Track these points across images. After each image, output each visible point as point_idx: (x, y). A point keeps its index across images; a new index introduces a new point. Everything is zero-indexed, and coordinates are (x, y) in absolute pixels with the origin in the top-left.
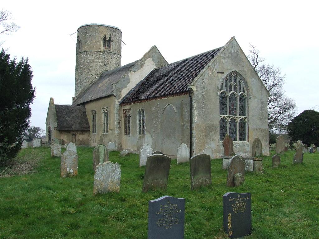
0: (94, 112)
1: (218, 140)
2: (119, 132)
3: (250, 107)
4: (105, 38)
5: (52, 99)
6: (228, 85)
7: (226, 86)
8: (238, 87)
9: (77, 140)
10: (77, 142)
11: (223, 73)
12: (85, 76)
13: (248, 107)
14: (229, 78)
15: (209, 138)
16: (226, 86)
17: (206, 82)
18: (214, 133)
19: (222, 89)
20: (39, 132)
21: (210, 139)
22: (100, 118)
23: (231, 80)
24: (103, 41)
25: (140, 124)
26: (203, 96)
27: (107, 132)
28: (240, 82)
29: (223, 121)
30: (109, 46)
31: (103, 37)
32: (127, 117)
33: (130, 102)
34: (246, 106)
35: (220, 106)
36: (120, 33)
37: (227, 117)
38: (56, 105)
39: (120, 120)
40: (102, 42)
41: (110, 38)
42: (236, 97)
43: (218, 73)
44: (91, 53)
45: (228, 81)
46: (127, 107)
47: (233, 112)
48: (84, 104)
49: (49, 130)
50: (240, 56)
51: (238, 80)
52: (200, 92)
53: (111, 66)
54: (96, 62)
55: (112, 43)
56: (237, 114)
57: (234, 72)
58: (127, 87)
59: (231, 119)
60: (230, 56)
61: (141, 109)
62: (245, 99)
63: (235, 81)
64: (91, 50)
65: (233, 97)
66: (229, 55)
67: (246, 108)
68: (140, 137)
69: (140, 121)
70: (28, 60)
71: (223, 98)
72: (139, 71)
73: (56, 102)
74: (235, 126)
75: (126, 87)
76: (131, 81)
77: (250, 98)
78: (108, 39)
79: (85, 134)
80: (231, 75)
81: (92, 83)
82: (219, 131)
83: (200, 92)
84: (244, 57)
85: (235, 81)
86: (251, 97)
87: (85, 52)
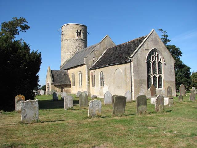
21: (142, 88)
25: (101, 80)
26: (138, 63)
32: (94, 77)
43: (146, 50)
69: (101, 78)
78: (79, 32)
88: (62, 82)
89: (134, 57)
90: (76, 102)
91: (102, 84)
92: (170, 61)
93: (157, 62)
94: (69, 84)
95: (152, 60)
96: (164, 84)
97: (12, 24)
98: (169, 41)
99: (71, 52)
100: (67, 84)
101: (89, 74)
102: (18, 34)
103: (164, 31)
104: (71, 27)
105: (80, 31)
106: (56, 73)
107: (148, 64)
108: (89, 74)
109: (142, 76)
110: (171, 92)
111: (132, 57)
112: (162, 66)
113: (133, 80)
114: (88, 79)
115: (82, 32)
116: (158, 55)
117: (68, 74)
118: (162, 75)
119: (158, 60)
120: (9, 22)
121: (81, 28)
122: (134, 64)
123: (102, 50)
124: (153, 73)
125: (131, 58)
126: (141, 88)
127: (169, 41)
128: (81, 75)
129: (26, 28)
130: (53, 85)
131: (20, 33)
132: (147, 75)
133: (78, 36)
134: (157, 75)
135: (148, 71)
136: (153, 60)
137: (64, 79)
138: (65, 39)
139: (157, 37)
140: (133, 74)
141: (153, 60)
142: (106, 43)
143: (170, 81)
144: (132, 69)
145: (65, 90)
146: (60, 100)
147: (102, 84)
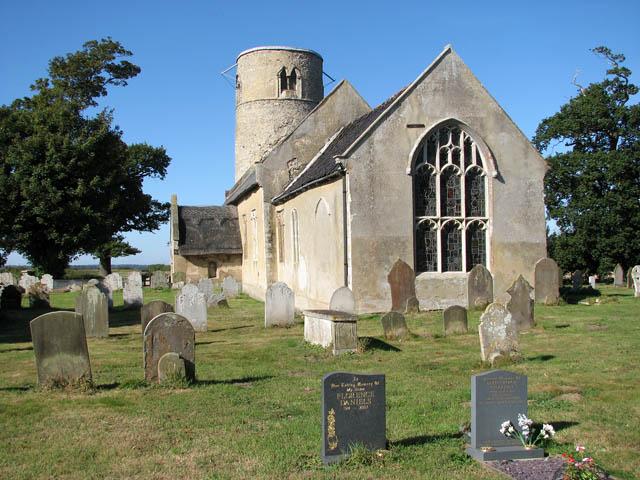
26: (372, 179)
43: (409, 126)
78: (288, 74)
88: (213, 246)
89: (353, 156)
91: (296, 259)
92: (526, 165)
93: (462, 171)
94: (234, 252)
95: (465, 168)
96: (492, 257)
97: (79, 61)
98: (633, 90)
100: (227, 252)
101: (271, 218)
102: (105, 93)
103: (614, 52)
104: (260, 59)
105: (293, 72)
106: (195, 216)
107: (421, 182)
108: (271, 218)
109: (388, 228)
110: (488, 289)
111: (346, 157)
112: (488, 185)
114: (270, 235)
115: (298, 75)
116: (468, 144)
117: (237, 219)
118: (485, 221)
119: (468, 162)
121: (296, 60)
122: (354, 181)
123: (324, 132)
124: (442, 215)
125: (343, 161)
127: (633, 90)
129: (127, 71)
130: (180, 257)
131: (108, 87)
132: (416, 221)
133: (284, 87)
134: (461, 221)
135: (421, 204)
136: (443, 160)
137: (219, 236)
138: (243, 101)
139: (463, 76)
141: (443, 160)
142: (338, 108)
143: (524, 243)
145: (222, 272)
146: (27, 309)
147: (296, 259)
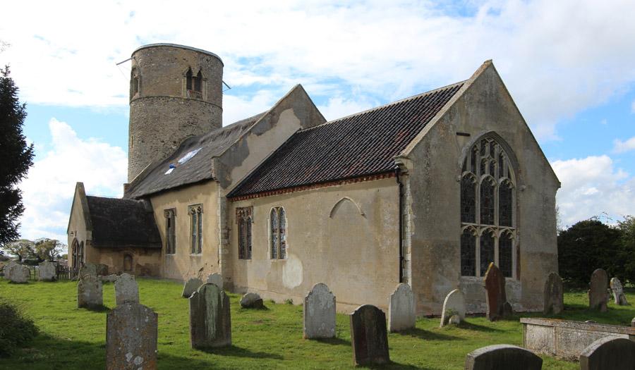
0: (171, 215)
1: (457, 275)
2: (227, 252)
3: (521, 209)
4: (190, 72)
5: (80, 187)
6: (478, 160)
7: (473, 162)
8: (497, 166)
9: (134, 266)
10: (134, 270)
11: (468, 135)
12: (149, 145)
13: (518, 208)
14: (479, 147)
15: (440, 270)
16: (473, 162)
17: (433, 152)
18: (451, 260)
19: (464, 169)
20: (57, 248)
21: (442, 273)
22: (184, 222)
23: (483, 153)
24: (186, 79)
25: (273, 237)
26: (428, 181)
27: (200, 251)
28: (501, 157)
29: (467, 237)
30: (198, 88)
31: (186, 69)
32: (245, 224)
33: (253, 194)
34: (514, 205)
35: (462, 204)
36: (220, 65)
37: (476, 227)
38: (88, 197)
39: (229, 230)
40: (184, 81)
41: (199, 73)
42: (493, 187)
43: (458, 134)
44: (161, 101)
45: (478, 152)
46: (244, 204)
47: (487, 218)
48: (148, 197)
49: (76, 246)
50: (503, 103)
51: (497, 150)
52: (421, 173)
53: (202, 127)
54: (172, 119)
55: (203, 82)
56: (495, 222)
57: (492, 135)
58: (243, 163)
59: (483, 233)
60: (483, 101)
61: (277, 208)
62: (511, 193)
63: (492, 152)
64: (160, 95)
65: (487, 188)
66: (481, 98)
67: (514, 210)
68: (274, 265)
69: (273, 231)
70: (10, 69)
71: (467, 188)
72: (268, 133)
73: (89, 191)
74: (492, 244)
75: (240, 164)
76: (250, 152)
77: (523, 190)
78: (195, 75)
79: (151, 255)
80: (483, 141)
81: (164, 159)
82: (460, 256)
83: (421, 173)
84: (510, 105)
85: (492, 152)
86: (524, 187)
87: (148, 97)
90: (333, 268)
99: (166, 139)
113: (408, 243)
120: (16, 100)
124: (482, 222)
126: (439, 276)
128: (197, 213)
135: (467, 214)
140: (409, 217)
144: (409, 198)
147: (278, 252)
